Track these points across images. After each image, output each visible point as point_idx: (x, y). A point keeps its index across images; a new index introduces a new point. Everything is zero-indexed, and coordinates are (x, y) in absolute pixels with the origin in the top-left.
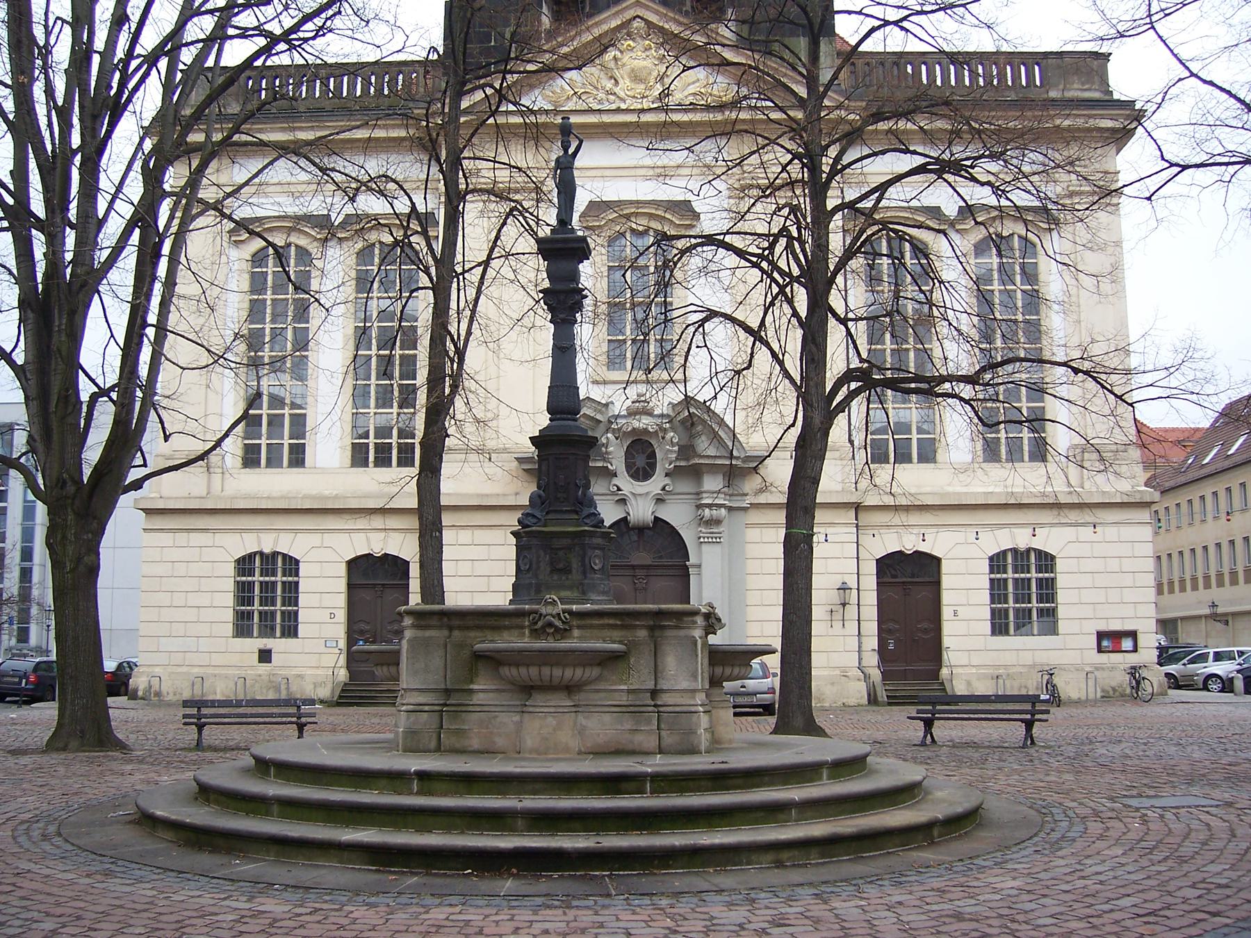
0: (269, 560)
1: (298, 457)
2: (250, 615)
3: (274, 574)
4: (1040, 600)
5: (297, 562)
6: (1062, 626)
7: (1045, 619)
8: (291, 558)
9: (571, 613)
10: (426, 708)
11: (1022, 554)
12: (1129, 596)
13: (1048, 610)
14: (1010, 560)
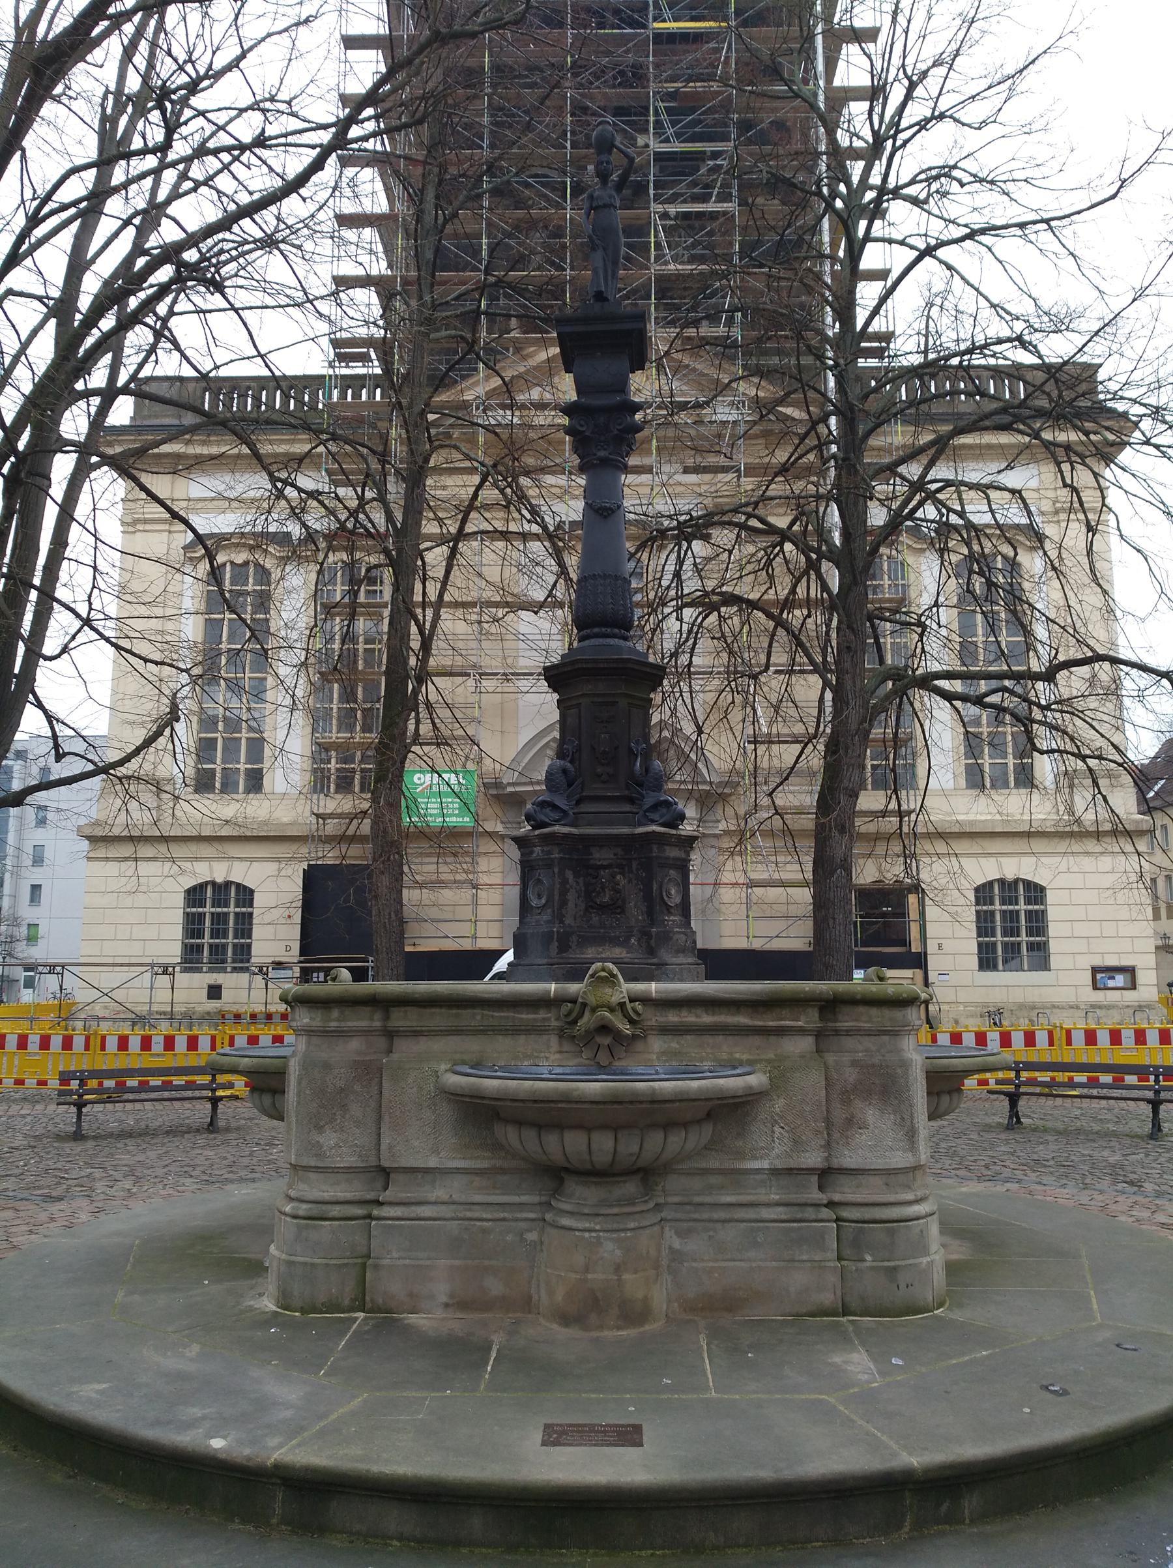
0: (221, 890)
1: (255, 782)
2: (199, 948)
3: (227, 905)
4: (1004, 934)
5: (252, 892)
6: (1054, 961)
7: (1035, 953)
8: (245, 887)
9: (646, 1000)
10: (336, 1211)
11: (1010, 884)
12: (1127, 930)
13: (1039, 944)
14: (996, 891)
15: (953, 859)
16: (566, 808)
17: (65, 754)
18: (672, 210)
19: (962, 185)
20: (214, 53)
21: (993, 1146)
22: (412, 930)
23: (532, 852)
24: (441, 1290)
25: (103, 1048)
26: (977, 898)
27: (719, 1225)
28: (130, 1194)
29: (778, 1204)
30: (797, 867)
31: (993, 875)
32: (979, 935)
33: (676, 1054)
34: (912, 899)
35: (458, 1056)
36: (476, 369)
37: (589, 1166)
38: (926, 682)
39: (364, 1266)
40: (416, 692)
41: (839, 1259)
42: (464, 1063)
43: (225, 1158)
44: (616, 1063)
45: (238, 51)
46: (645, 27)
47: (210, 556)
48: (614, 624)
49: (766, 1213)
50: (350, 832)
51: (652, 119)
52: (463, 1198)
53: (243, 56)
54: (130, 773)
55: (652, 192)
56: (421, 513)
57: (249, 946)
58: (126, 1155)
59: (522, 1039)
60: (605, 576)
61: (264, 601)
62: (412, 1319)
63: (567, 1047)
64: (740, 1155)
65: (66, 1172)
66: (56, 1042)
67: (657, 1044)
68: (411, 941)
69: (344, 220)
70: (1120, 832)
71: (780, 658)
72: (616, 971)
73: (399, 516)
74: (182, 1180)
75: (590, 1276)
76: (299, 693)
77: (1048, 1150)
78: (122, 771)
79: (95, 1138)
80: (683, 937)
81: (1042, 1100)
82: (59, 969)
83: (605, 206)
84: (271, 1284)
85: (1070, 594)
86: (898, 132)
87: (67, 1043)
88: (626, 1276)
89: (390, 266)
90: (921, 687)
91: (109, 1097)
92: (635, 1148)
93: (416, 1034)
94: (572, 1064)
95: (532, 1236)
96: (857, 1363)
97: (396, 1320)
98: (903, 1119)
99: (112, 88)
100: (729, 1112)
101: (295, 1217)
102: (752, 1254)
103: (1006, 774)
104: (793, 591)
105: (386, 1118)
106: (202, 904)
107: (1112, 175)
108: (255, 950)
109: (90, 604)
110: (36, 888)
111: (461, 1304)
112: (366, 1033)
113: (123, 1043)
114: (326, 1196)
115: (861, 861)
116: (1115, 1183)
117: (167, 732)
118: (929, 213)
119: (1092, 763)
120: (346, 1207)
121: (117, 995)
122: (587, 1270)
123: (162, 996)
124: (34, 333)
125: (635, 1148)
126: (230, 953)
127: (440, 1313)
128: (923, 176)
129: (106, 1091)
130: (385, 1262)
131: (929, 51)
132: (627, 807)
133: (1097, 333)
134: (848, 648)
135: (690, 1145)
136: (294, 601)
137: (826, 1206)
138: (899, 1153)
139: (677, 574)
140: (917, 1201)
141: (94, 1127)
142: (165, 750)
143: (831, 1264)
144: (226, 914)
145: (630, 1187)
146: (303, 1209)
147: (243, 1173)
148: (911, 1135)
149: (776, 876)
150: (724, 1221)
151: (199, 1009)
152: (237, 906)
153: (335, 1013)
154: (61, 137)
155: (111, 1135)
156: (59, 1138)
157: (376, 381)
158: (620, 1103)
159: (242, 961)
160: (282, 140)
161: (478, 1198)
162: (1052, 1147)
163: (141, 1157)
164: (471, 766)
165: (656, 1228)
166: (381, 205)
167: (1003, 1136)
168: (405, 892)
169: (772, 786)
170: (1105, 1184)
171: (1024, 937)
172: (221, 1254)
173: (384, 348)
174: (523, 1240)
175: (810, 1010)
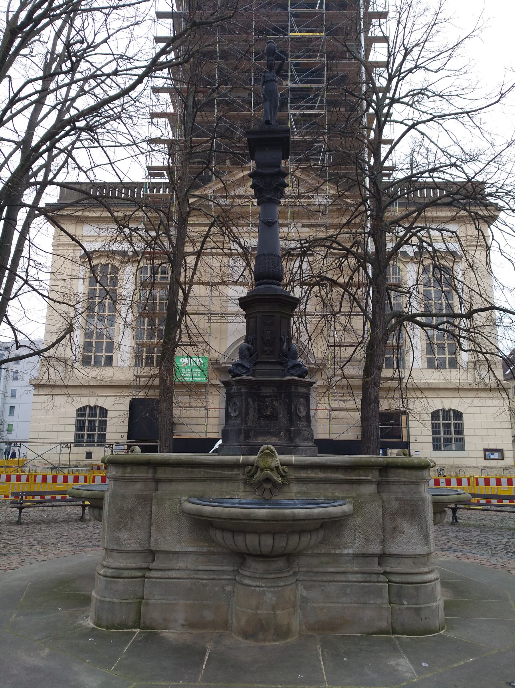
0: (93, 409)
1: (109, 361)
2: (82, 436)
3: (95, 416)
4: (444, 434)
5: (107, 411)
6: (467, 446)
7: (458, 443)
8: (104, 408)
9: (289, 465)
10: (126, 573)
11: (447, 412)
12: (499, 432)
13: (460, 438)
15: (425, 400)
16: (249, 367)
17: (21, 346)
18: (298, 112)
19: (428, 98)
20: (95, 35)
21: (446, 533)
22: (178, 429)
23: (232, 389)
24: (181, 617)
25: (35, 481)
26: (432, 417)
27: (326, 584)
28: (39, 552)
29: (357, 573)
30: (354, 402)
31: (439, 407)
32: (433, 434)
33: (305, 493)
34: (403, 417)
35: (191, 493)
36: (211, 181)
37: (259, 553)
38: (412, 318)
39: (140, 603)
40: (181, 319)
41: (390, 603)
42: (194, 496)
43: (87, 535)
44: (274, 498)
45: (107, 36)
46: (287, 35)
47: (90, 260)
48: (273, 278)
49: (351, 578)
50: (150, 383)
51: (289, 74)
52: (193, 568)
53: (109, 37)
54: (50, 355)
55: (289, 104)
56: (184, 239)
57: (105, 435)
58: (40, 532)
59: (225, 484)
60: (269, 255)
61: (115, 280)
62: (165, 633)
63: (248, 489)
64: (338, 547)
65: (10, 541)
66: (14, 478)
67: (295, 488)
68: (178, 434)
69: (154, 115)
70: (501, 388)
71: (346, 308)
72: (274, 450)
73: (174, 241)
74: (65, 546)
75: (259, 612)
76: (128, 320)
77: (472, 535)
78: (46, 354)
79: (27, 524)
80: (307, 433)
81: (466, 511)
82: (18, 444)
83: (271, 80)
84: (92, 611)
85: (479, 279)
86: (400, 74)
87: (19, 479)
88: (278, 612)
89: (174, 136)
90: (408, 320)
91: (36, 504)
92: (284, 544)
93: (170, 481)
94: (251, 498)
95: (228, 588)
96: (403, 665)
97: (156, 634)
98: (422, 528)
99: (50, 50)
100: (332, 525)
101: (105, 576)
102: (344, 600)
103: (445, 362)
104: (351, 278)
105: (154, 525)
106: (84, 416)
107: (497, 92)
108: (107, 437)
109: (27, 273)
110: (12, 408)
111: (191, 625)
112: (144, 480)
113: (44, 479)
114: (122, 565)
115: (383, 400)
116: (507, 553)
117: (68, 336)
118: (414, 108)
119: (488, 356)
120: (132, 571)
121: (44, 456)
122: (257, 608)
123: (65, 457)
124: (11, 155)
125: (284, 544)
126: (96, 438)
127: (180, 630)
128: (412, 93)
129: (36, 502)
130: (151, 601)
131: (416, 37)
132: (279, 367)
133: (491, 161)
134: (378, 302)
135: (313, 542)
136: (128, 280)
137: (382, 574)
138: (421, 546)
139: (300, 267)
140: (430, 572)
141: (28, 518)
142: (66, 345)
143: (385, 606)
144: (95, 421)
145: (281, 563)
146: (110, 572)
147: (93, 542)
148: (426, 536)
149: (344, 406)
150: (329, 582)
151: (82, 463)
152: (100, 417)
153: (129, 470)
154: (26, 69)
155: (35, 522)
156: (11, 523)
157: (166, 185)
158: (277, 521)
159: (101, 442)
160: (125, 72)
161: (201, 567)
162: (474, 534)
163: (47, 534)
164: (206, 355)
165: (294, 585)
166: (171, 110)
167: (450, 528)
168: (174, 412)
169: (342, 364)
170: (502, 553)
171: (453, 435)
172: (68, 592)
173: (169, 170)
174: (224, 590)
175: (374, 471)
